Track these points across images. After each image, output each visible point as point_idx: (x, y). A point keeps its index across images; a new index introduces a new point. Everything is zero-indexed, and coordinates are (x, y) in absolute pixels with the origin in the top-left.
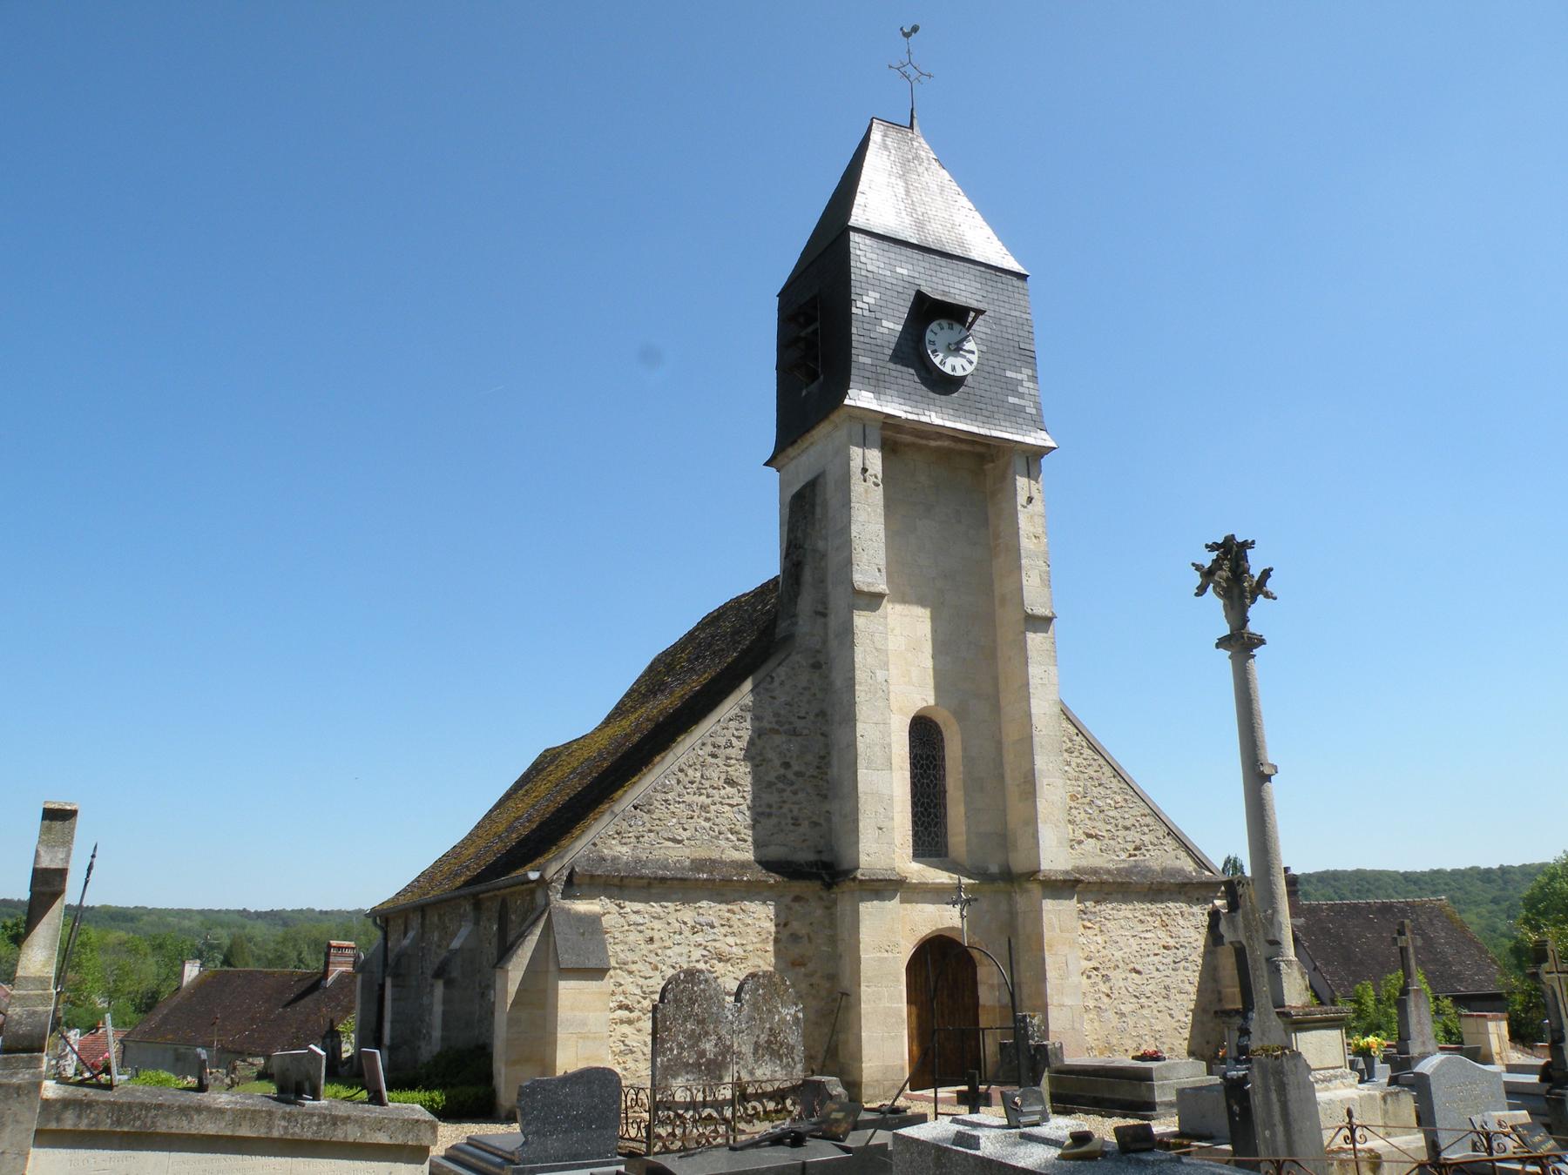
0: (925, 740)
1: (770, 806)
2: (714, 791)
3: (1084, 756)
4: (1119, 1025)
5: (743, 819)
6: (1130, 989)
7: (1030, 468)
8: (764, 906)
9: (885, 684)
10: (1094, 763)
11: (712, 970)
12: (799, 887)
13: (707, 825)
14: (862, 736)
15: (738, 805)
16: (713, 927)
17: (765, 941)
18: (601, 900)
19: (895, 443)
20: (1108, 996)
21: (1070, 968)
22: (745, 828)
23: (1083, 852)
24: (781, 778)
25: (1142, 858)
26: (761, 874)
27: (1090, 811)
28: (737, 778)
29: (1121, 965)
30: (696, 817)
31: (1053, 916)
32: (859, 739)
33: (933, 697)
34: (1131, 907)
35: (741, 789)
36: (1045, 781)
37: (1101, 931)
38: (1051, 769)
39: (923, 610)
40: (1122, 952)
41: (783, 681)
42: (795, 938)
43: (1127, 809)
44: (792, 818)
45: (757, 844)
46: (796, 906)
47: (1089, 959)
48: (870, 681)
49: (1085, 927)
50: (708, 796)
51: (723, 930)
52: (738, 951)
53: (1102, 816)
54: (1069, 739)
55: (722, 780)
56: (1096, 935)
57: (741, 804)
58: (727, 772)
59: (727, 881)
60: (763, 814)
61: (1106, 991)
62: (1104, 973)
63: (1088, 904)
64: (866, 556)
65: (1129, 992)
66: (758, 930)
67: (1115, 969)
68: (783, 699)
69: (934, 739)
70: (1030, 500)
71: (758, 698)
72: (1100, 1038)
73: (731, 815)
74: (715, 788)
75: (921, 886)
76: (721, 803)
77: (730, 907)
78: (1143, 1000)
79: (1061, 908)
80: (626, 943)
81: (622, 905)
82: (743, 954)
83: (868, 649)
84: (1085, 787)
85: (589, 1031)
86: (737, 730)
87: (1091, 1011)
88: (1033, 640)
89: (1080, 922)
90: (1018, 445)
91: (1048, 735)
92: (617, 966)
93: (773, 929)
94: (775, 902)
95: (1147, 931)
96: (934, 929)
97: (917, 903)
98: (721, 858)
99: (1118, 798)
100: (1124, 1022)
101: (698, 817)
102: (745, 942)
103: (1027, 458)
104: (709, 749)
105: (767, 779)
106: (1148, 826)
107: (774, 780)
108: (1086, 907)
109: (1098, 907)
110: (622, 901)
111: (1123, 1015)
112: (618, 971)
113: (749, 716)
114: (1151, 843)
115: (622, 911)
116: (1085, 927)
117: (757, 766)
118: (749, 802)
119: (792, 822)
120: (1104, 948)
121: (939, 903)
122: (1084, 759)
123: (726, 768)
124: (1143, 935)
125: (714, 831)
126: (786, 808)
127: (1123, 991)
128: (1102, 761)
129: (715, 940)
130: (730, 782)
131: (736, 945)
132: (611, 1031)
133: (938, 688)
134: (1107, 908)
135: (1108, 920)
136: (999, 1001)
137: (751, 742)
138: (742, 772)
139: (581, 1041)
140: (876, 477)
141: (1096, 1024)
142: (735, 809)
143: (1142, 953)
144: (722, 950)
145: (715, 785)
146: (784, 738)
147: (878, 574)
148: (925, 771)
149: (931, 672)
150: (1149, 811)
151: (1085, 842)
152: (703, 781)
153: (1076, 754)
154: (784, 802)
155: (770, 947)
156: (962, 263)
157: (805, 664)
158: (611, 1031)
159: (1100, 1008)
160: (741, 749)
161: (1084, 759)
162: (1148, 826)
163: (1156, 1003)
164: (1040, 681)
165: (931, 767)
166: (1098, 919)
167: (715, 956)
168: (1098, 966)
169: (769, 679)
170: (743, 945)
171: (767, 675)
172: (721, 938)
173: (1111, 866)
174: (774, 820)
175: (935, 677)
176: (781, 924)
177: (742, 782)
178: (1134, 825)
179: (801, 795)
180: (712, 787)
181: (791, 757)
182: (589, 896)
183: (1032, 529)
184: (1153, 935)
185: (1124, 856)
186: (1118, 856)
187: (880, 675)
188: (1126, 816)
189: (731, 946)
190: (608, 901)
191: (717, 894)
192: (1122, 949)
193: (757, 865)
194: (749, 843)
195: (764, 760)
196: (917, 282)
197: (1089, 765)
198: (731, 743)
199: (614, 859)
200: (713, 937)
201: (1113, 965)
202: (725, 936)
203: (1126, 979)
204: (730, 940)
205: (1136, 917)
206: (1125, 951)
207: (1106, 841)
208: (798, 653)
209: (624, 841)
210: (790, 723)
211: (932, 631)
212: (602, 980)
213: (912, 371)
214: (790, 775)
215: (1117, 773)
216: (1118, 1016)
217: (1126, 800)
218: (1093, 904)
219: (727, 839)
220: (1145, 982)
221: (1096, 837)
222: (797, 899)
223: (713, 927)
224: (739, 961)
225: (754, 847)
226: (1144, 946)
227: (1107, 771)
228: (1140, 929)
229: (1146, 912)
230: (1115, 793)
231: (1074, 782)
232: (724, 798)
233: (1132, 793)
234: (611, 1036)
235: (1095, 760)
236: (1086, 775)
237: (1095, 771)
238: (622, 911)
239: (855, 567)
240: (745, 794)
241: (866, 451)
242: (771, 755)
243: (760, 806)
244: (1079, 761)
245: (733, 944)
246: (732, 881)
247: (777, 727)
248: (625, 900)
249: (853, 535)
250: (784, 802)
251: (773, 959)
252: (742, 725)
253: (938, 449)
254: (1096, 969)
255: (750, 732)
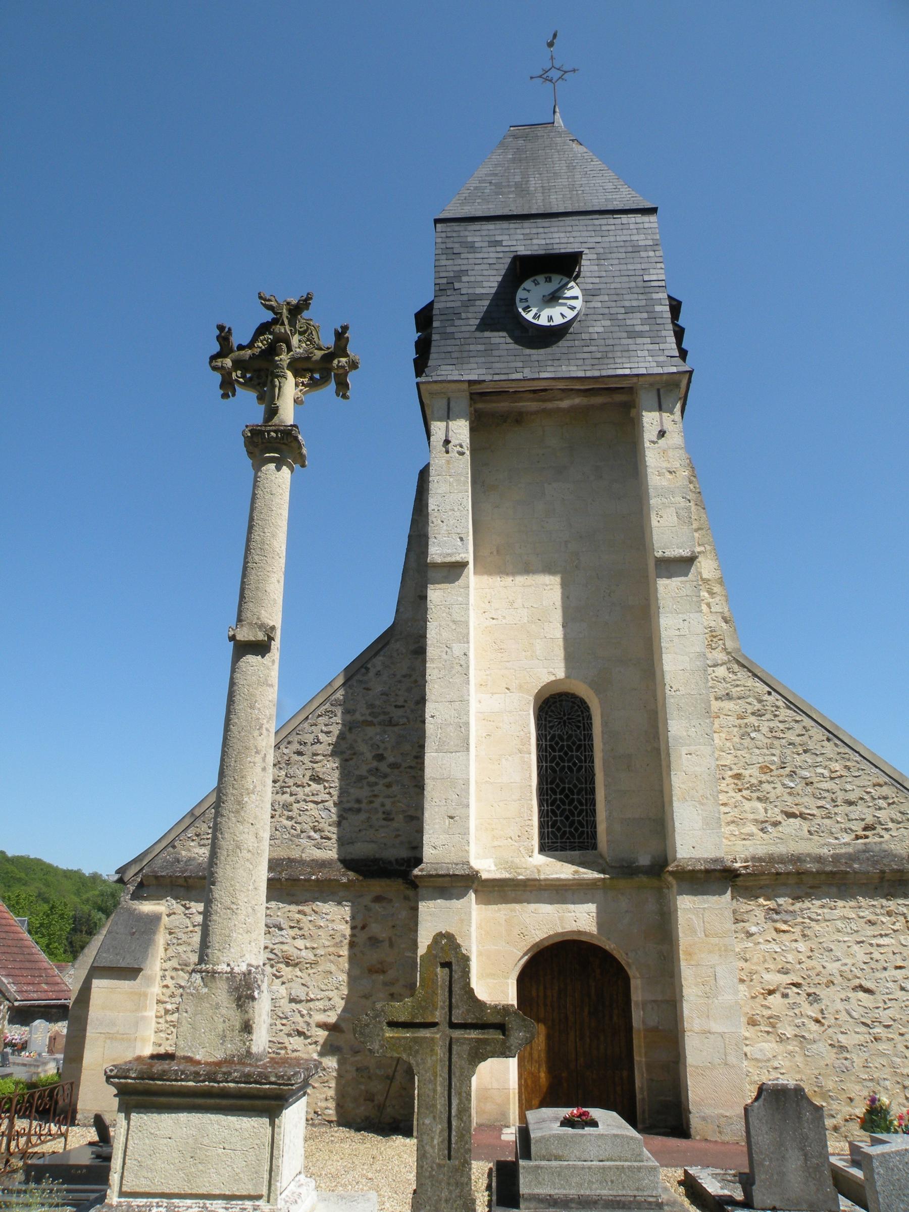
0: (565, 718)
1: (358, 801)
2: (298, 789)
3: (781, 718)
4: (837, 1063)
5: (327, 816)
6: (854, 1014)
7: (663, 400)
8: (340, 907)
9: (464, 657)
10: (796, 726)
11: (278, 974)
12: (378, 886)
13: (289, 823)
14: (432, 717)
15: (323, 802)
16: (281, 929)
17: (338, 945)
18: (167, 901)
19: (520, 414)
20: (817, 1021)
21: (721, 983)
22: (330, 825)
23: (779, 835)
24: (375, 771)
25: (877, 839)
26: (346, 877)
27: (792, 785)
28: (323, 774)
29: (838, 980)
30: (277, 816)
31: (693, 917)
32: (428, 719)
33: (563, 669)
34: (853, 903)
35: (327, 785)
36: (684, 750)
37: (804, 936)
38: (694, 735)
39: (552, 577)
40: (840, 962)
41: (379, 671)
42: (374, 941)
43: (849, 779)
44: (384, 813)
45: (342, 842)
46: (377, 907)
47: (784, 971)
48: (445, 656)
49: (777, 931)
50: (291, 795)
51: (292, 933)
52: (309, 955)
53: (809, 789)
54: (757, 699)
55: (307, 777)
56: (796, 941)
57: (327, 801)
58: (313, 769)
59: (295, 880)
60: (350, 809)
61: (814, 1015)
62: (811, 991)
63: (781, 901)
64: (445, 528)
65: (852, 1017)
66: (332, 932)
67: (828, 987)
68: (379, 689)
69: (579, 716)
70: (662, 434)
71: (351, 691)
72: (804, 1078)
73: (315, 813)
74: (298, 786)
75: (532, 883)
76: (305, 801)
77: (300, 908)
78: (878, 1030)
79: (706, 906)
80: (189, 944)
81: (188, 906)
82: (313, 958)
83: (443, 623)
84: (783, 755)
85: (118, 1033)
86: (326, 725)
87: (790, 1042)
88: (666, 587)
89: (770, 924)
90: (641, 379)
91: (690, 694)
92: (179, 967)
93: (348, 932)
94: (353, 903)
95: (881, 935)
96: (551, 933)
97: (529, 903)
98: (301, 856)
99: (836, 766)
100: (846, 1059)
101: (280, 816)
102: (315, 946)
103: (658, 390)
104: (295, 746)
105: (357, 773)
106: (885, 798)
107: (365, 773)
108: (779, 905)
109: (798, 905)
110: (187, 902)
111: (843, 1048)
112: (180, 972)
113: (339, 711)
114: (892, 821)
115: (187, 912)
116: (777, 931)
117: (346, 760)
118: (335, 798)
119: (384, 816)
120: (809, 957)
121: (557, 903)
122: (780, 722)
123: (312, 764)
124: (874, 941)
125: (295, 830)
126: (378, 801)
127: (843, 1016)
128: (808, 722)
129: (282, 943)
130: (316, 779)
131: (306, 948)
132: (168, 1034)
133: (570, 658)
134: (813, 906)
135: (817, 921)
136: (643, 1022)
137: (341, 737)
138: (330, 768)
139: (108, 1041)
140: (461, 446)
141: (799, 1059)
142: (321, 806)
143: (873, 964)
144: (290, 953)
145: (299, 783)
146: (378, 729)
147: (459, 543)
148: (566, 754)
149: (561, 642)
150: (887, 779)
151: (784, 823)
152: (287, 780)
153: (768, 716)
154: (375, 796)
155: (345, 952)
156: (571, 218)
157: (404, 651)
158: (168, 1034)
159: (803, 1037)
160: (329, 744)
161: (780, 722)
162: (885, 798)
163: (902, 1035)
164: (677, 633)
165: (574, 748)
166: (800, 920)
167: (281, 960)
168: (800, 981)
169: (363, 670)
170: (313, 948)
171: (362, 667)
172: (289, 940)
173: (824, 851)
174: (363, 816)
175: (566, 648)
176: (358, 926)
177: (329, 778)
178: (862, 799)
179: (395, 789)
180: (295, 784)
181: (386, 749)
182: (158, 897)
183: (665, 465)
184: (893, 941)
185: (847, 838)
186: (836, 838)
187: (457, 649)
188: (849, 787)
189: (300, 950)
190: (174, 902)
191: (288, 895)
192: (839, 960)
193: (339, 863)
194: (334, 841)
195: (354, 754)
196: (513, 249)
197: (789, 729)
198: (318, 740)
199: (190, 859)
200: (280, 939)
201: (825, 981)
202: (294, 938)
203: (847, 999)
204: (300, 943)
205: (863, 917)
206: (844, 961)
207: (818, 821)
208: (397, 640)
209: (202, 842)
210: (385, 713)
211: (562, 598)
212: (135, 980)
213: (505, 334)
214: (383, 767)
215: (832, 735)
216: (835, 1050)
217: (848, 768)
218: (790, 901)
219: (309, 837)
220: (881, 1005)
221: (802, 816)
222: (378, 899)
223: (281, 929)
224: (308, 965)
225: (339, 845)
226: (876, 955)
227: (818, 734)
228: (869, 933)
229: (878, 911)
230: (830, 759)
231: (765, 751)
232: (308, 796)
233: (858, 758)
234: (167, 1039)
235: (797, 721)
236: (784, 741)
237: (799, 735)
238: (187, 912)
239: (431, 541)
240: (331, 790)
241: (450, 423)
242: (363, 748)
243: (348, 802)
244: (772, 724)
245: (303, 947)
246: (300, 880)
247: (370, 719)
248: (190, 901)
249: (430, 509)
250: (375, 796)
251: (347, 965)
252: (331, 720)
253: (572, 410)
254: (797, 985)
255: (340, 726)
